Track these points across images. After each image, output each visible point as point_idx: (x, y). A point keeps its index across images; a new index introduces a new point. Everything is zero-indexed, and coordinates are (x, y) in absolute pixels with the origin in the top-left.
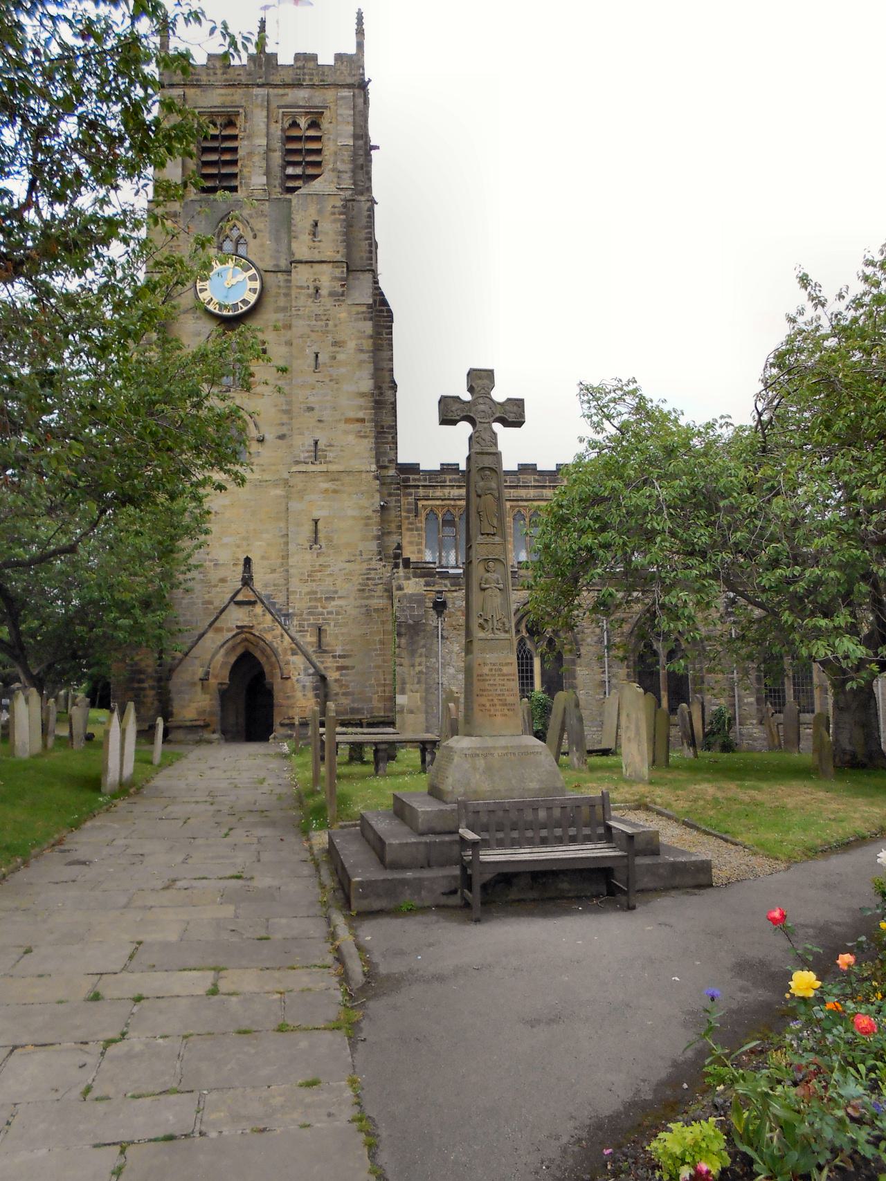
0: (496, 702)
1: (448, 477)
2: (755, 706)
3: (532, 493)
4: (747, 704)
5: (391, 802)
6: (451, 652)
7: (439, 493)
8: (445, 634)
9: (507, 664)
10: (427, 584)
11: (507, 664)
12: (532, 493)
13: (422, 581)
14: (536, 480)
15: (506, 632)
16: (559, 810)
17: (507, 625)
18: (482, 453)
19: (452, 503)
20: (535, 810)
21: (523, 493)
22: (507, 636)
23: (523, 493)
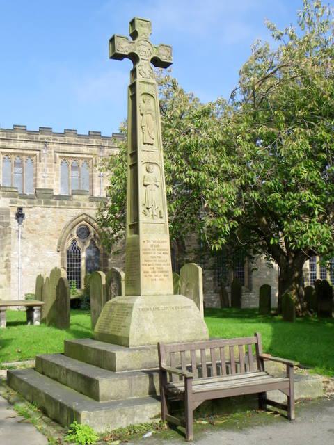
0: (156, 269)
1: (19, 135)
2: (213, 283)
3: (73, 149)
4: (208, 281)
5: (63, 343)
6: (27, 248)
7: (12, 144)
8: (23, 236)
9: (163, 242)
10: (12, 202)
11: (163, 242)
12: (73, 149)
13: (8, 200)
14: (76, 141)
15: (161, 217)
16: (218, 348)
17: (163, 213)
18: (143, 82)
19: (21, 151)
20: (192, 351)
21: (67, 148)
22: (162, 221)
23: (67, 148)
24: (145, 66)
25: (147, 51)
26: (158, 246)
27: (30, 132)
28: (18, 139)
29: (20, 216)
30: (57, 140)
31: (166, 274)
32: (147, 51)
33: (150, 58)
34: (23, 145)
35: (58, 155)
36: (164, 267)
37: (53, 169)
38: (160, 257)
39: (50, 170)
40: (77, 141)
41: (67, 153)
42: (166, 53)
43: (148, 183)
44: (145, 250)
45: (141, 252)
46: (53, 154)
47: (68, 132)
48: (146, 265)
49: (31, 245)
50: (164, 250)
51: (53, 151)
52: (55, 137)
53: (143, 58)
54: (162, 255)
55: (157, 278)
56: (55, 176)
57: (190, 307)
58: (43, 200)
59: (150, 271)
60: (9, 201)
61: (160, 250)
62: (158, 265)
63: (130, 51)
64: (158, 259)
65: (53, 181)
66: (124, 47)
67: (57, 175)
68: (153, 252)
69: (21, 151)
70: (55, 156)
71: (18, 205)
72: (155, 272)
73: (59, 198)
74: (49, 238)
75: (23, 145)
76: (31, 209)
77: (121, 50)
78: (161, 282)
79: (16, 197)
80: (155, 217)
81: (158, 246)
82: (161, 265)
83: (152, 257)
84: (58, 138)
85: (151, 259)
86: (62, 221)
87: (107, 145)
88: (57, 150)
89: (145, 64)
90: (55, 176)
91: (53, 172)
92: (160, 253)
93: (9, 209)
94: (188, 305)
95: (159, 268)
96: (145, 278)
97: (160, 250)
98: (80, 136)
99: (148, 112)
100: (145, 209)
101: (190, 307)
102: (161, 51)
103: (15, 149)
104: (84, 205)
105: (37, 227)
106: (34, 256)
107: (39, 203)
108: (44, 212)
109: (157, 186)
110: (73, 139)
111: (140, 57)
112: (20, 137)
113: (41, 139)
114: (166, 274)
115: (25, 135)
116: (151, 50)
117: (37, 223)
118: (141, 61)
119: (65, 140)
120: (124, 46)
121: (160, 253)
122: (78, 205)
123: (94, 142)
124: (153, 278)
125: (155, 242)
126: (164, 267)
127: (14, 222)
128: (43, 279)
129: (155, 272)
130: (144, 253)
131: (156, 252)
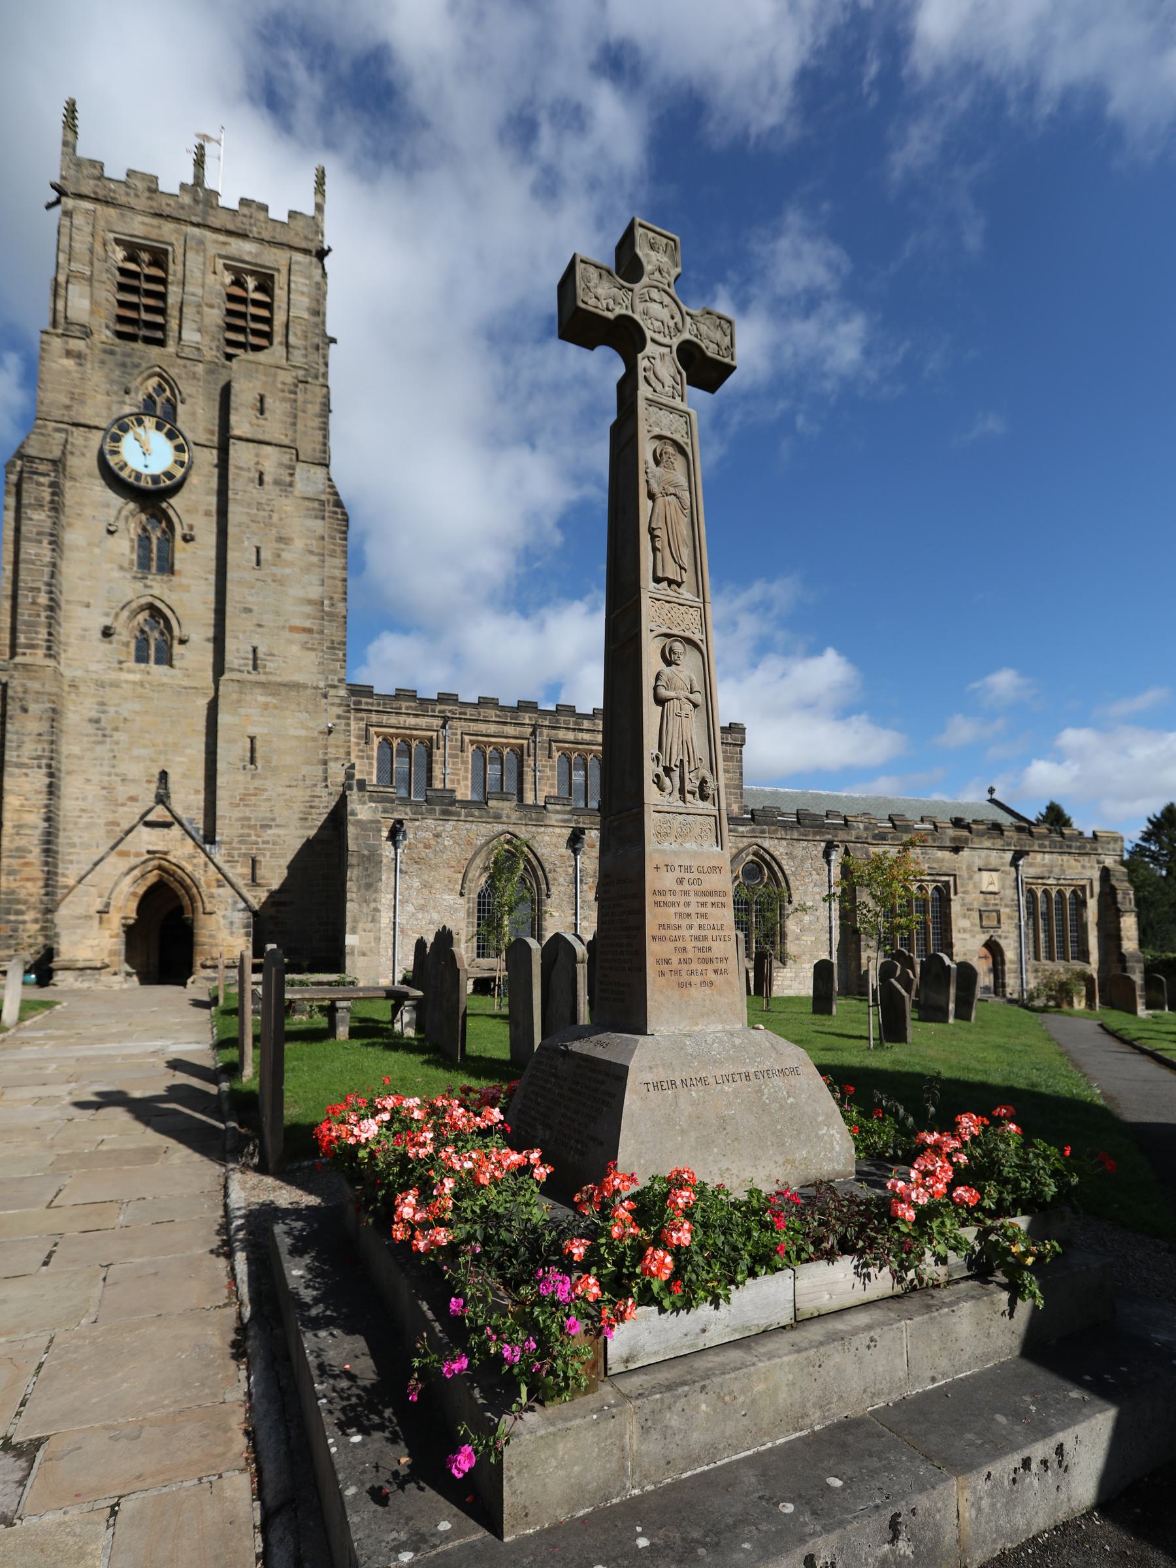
1: (404, 704)
3: (493, 729)
7: (393, 720)
9: (714, 869)
11: (714, 869)
12: (493, 729)
15: (704, 797)
17: (711, 784)
19: (408, 732)
21: (482, 727)
23: (482, 727)
24: (659, 364)
25: (667, 319)
26: (698, 881)
27: (424, 701)
28: (403, 711)
29: (396, 833)
30: (465, 714)
31: (722, 966)
32: (667, 319)
33: (675, 342)
34: (412, 721)
35: (467, 738)
36: (715, 945)
37: (459, 760)
38: (705, 916)
39: (454, 763)
40: (498, 716)
41: (482, 735)
42: (717, 336)
43: (671, 694)
44: (661, 892)
45: (649, 899)
46: (459, 737)
47: (484, 702)
48: (662, 938)
49: (416, 884)
50: (716, 893)
51: (459, 732)
52: (463, 710)
53: (657, 337)
54: (709, 910)
55: (696, 979)
56: (462, 773)
57: (794, 1071)
58: (437, 808)
59: (675, 959)
60: (381, 809)
61: (703, 894)
62: (697, 938)
63: (619, 311)
64: (696, 922)
65: (458, 781)
66: (602, 296)
67: (466, 770)
68: (683, 899)
69: (408, 732)
70: (462, 741)
71: (397, 816)
72: (687, 961)
73: (465, 804)
74: (449, 872)
75: (412, 721)
76: (417, 823)
77: (592, 301)
78: (708, 991)
79: (392, 801)
80: (689, 797)
81: (698, 881)
82: (705, 938)
83: (681, 915)
84: (468, 711)
85: (677, 921)
86: (470, 843)
87: (547, 723)
88: (466, 730)
89: (662, 356)
90: (462, 773)
91: (460, 766)
92: (704, 904)
93: (379, 822)
94: (790, 1063)
95: (701, 949)
96: (662, 981)
97: (703, 894)
98: (504, 709)
99: (672, 490)
100: (660, 770)
101: (794, 1071)
102: (703, 329)
103: (398, 728)
104: (508, 817)
105: (424, 853)
106: (422, 902)
107: (431, 812)
108: (440, 829)
109: (695, 706)
110: (492, 714)
111: (649, 334)
112: (407, 708)
113: (440, 712)
114: (722, 966)
115: (413, 704)
116: (678, 318)
117: (427, 846)
118: (650, 348)
119: (479, 713)
120: (600, 291)
121: (704, 904)
122: (497, 817)
123: (527, 718)
124: (685, 978)
125: (688, 869)
126: (715, 945)
127: (387, 849)
128: (425, 945)
129: (687, 961)
130: (725, 894)
131: (693, 899)
